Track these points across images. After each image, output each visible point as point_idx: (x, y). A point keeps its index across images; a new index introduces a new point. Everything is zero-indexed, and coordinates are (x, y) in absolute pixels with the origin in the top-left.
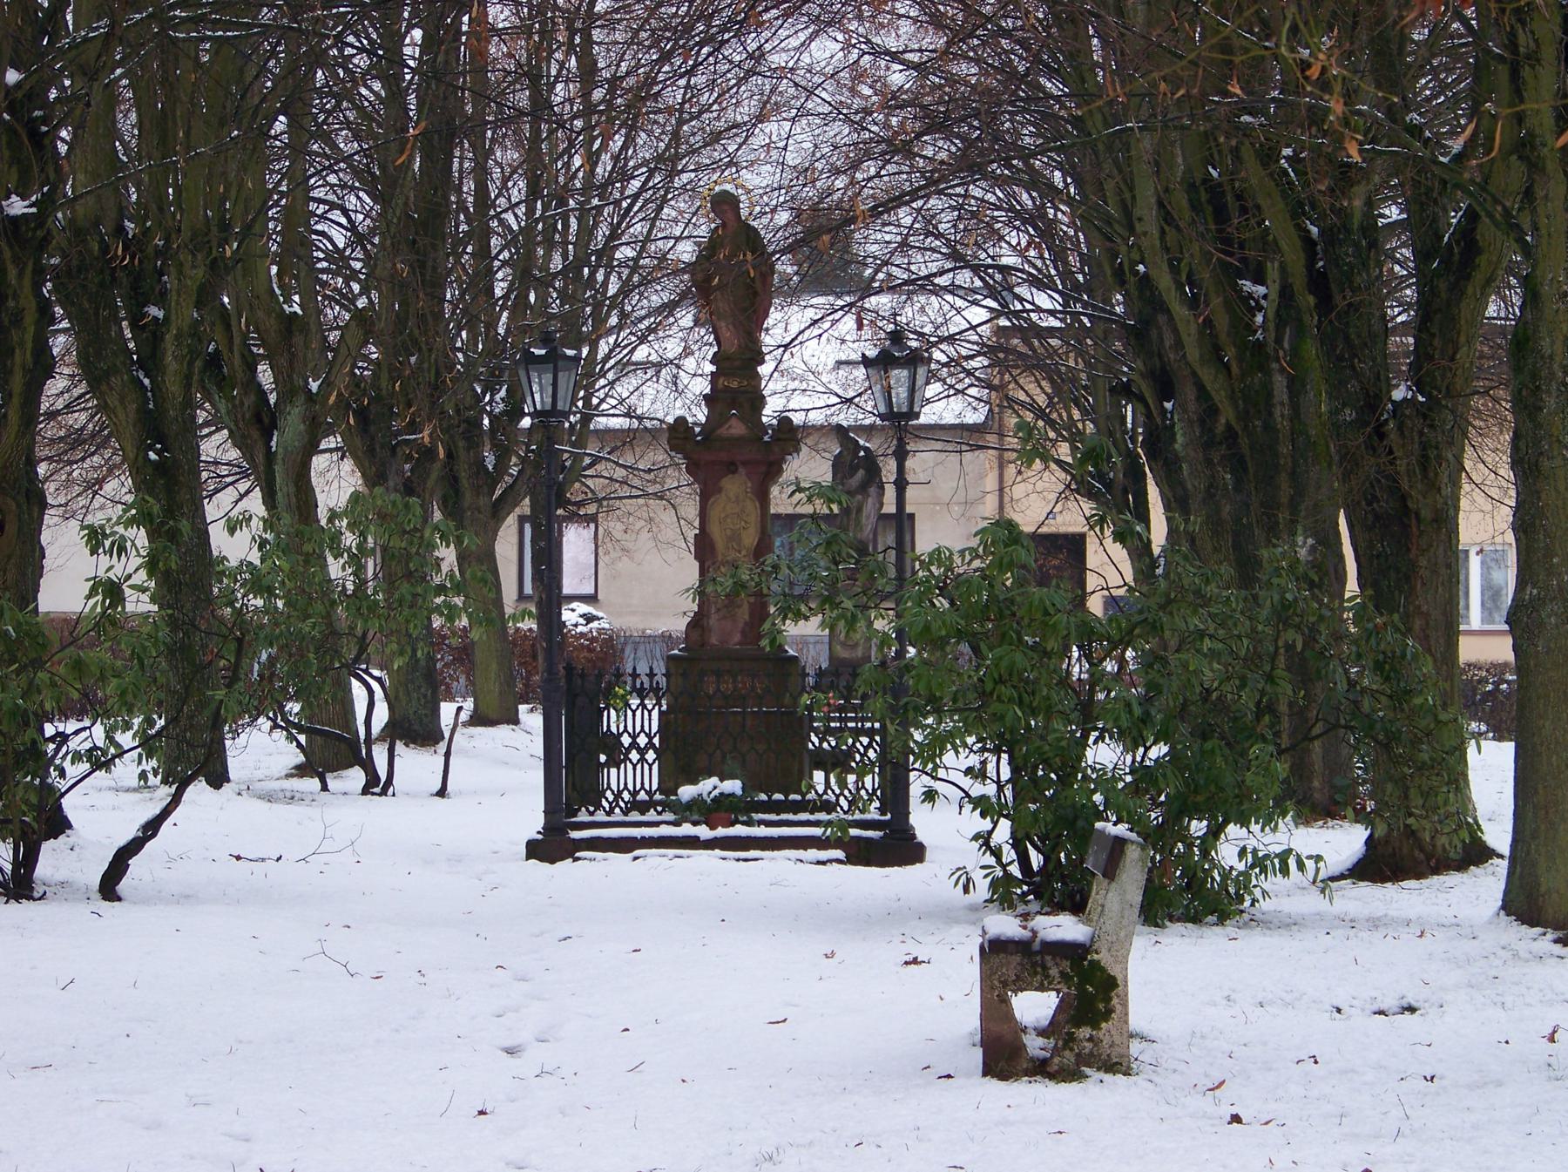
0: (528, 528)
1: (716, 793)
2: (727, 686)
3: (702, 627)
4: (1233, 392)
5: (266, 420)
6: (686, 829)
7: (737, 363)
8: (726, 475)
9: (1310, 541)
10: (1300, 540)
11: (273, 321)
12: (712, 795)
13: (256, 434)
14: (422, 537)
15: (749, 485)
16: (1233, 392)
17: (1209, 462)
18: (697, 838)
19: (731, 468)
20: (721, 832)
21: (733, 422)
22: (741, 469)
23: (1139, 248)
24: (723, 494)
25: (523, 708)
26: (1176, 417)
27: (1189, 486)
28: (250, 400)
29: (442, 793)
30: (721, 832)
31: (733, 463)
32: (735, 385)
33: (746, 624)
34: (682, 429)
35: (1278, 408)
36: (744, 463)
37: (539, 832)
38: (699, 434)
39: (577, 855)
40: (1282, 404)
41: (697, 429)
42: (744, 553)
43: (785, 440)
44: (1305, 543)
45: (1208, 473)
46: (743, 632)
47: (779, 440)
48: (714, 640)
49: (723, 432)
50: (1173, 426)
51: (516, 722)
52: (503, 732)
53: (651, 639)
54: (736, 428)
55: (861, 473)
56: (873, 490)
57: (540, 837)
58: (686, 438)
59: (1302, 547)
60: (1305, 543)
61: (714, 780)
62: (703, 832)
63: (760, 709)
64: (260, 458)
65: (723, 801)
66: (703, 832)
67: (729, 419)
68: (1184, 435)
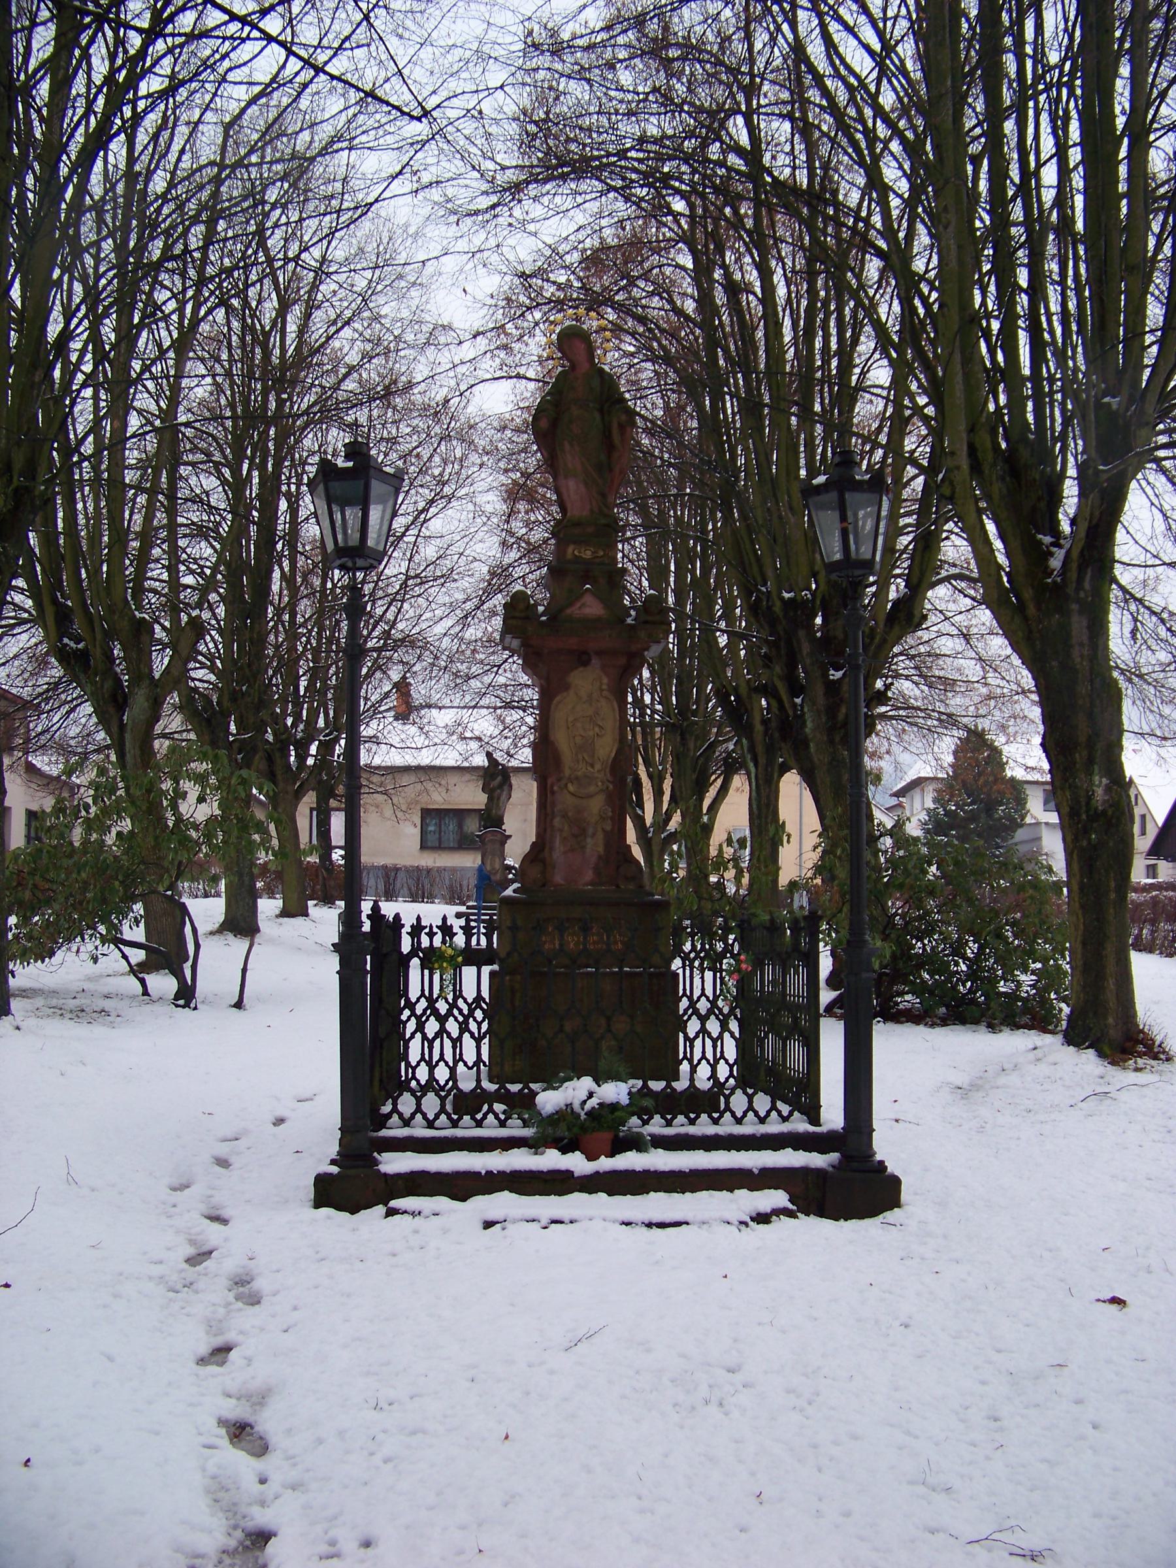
0: (315, 813)
1: (593, 1103)
2: (572, 942)
3: (543, 862)
4: (1031, 632)
5: (120, 700)
6: (551, 1160)
7: (590, 530)
8: (576, 668)
9: (1105, 781)
10: (1096, 779)
11: (126, 623)
12: (588, 1106)
13: (112, 710)
14: (229, 784)
15: (605, 680)
16: (1031, 632)
17: (831, 742)
18: (568, 1174)
19: (582, 659)
20: (605, 1164)
21: (588, 599)
22: (595, 661)
23: (951, 483)
24: (571, 692)
25: (311, 903)
26: (806, 710)
27: (816, 760)
28: (108, 684)
29: (239, 1005)
30: (605, 1164)
31: (585, 653)
32: (588, 554)
33: (600, 857)
34: (522, 606)
35: (1077, 648)
36: (599, 653)
37: (333, 1162)
38: (543, 614)
39: (394, 1203)
40: (1081, 645)
41: (541, 609)
42: (598, 766)
43: (654, 623)
44: (1101, 782)
45: (831, 750)
46: (596, 870)
47: (646, 622)
48: (558, 879)
49: (574, 611)
50: (803, 714)
51: (307, 915)
52: (299, 921)
53: (377, 868)
54: (591, 607)
55: (499, 778)
56: (506, 788)
57: (335, 1169)
58: (527, 618)
59: (1099, 786)
60: (1101, 782)
61: (587, 1082)
62: (577, 1163)
63: (621, 968)
64: (115, 729)
65: (608, 1113)
66: (577, 1163)
67: (582, 595)
68: (813, 721)
